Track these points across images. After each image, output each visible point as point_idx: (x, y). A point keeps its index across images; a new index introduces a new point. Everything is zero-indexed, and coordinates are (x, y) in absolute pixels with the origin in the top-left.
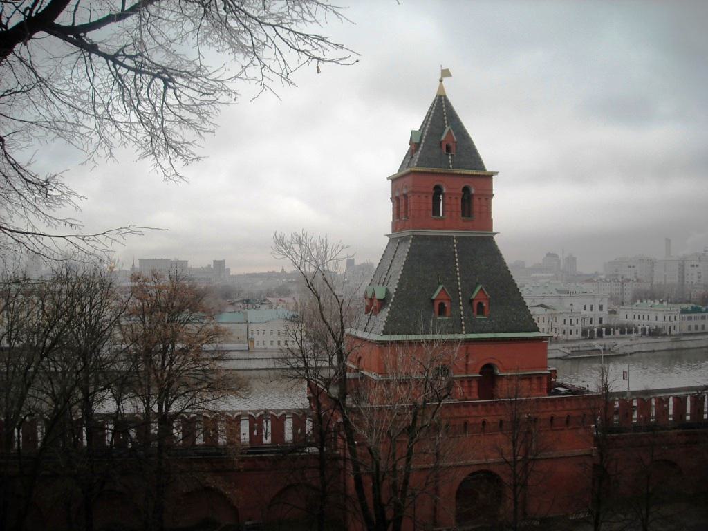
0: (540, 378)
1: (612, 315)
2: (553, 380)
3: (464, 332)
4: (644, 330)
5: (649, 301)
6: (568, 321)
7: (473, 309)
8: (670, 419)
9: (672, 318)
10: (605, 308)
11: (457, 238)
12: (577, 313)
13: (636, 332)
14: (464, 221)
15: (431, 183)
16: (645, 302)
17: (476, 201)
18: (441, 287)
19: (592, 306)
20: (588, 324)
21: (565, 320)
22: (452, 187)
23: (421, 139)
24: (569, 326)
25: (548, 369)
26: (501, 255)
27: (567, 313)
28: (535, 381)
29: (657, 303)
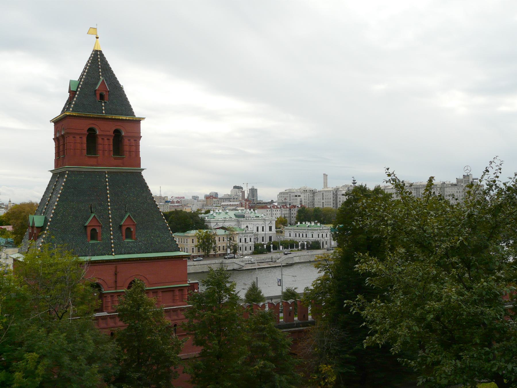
0: (182, 290)
1: (280, 234)
2: (196, 291)
3: (113, 254)
4: (303, 245)
5: (307, 223)
6: (243, 240)
7: (122, 233)
8: (281, 320)
9: (324, 235)
10: (273, 228)
11: (109, 173)
12: (250, 233)
13: (297, 246)
14: (115, 159)
15: (84, 126)
16: (304, 223)
17: (126, 141)
18: (93, 215)
19: (263, 227)
20: (260, 241)
21: (240, 239)
22: (105, 130)
23: (78, 87)
24: (244, 244)
25: (188, 282)
26: (148, 187)
27: (243, 234)
28: (177, 293)
29: (313, 224)
